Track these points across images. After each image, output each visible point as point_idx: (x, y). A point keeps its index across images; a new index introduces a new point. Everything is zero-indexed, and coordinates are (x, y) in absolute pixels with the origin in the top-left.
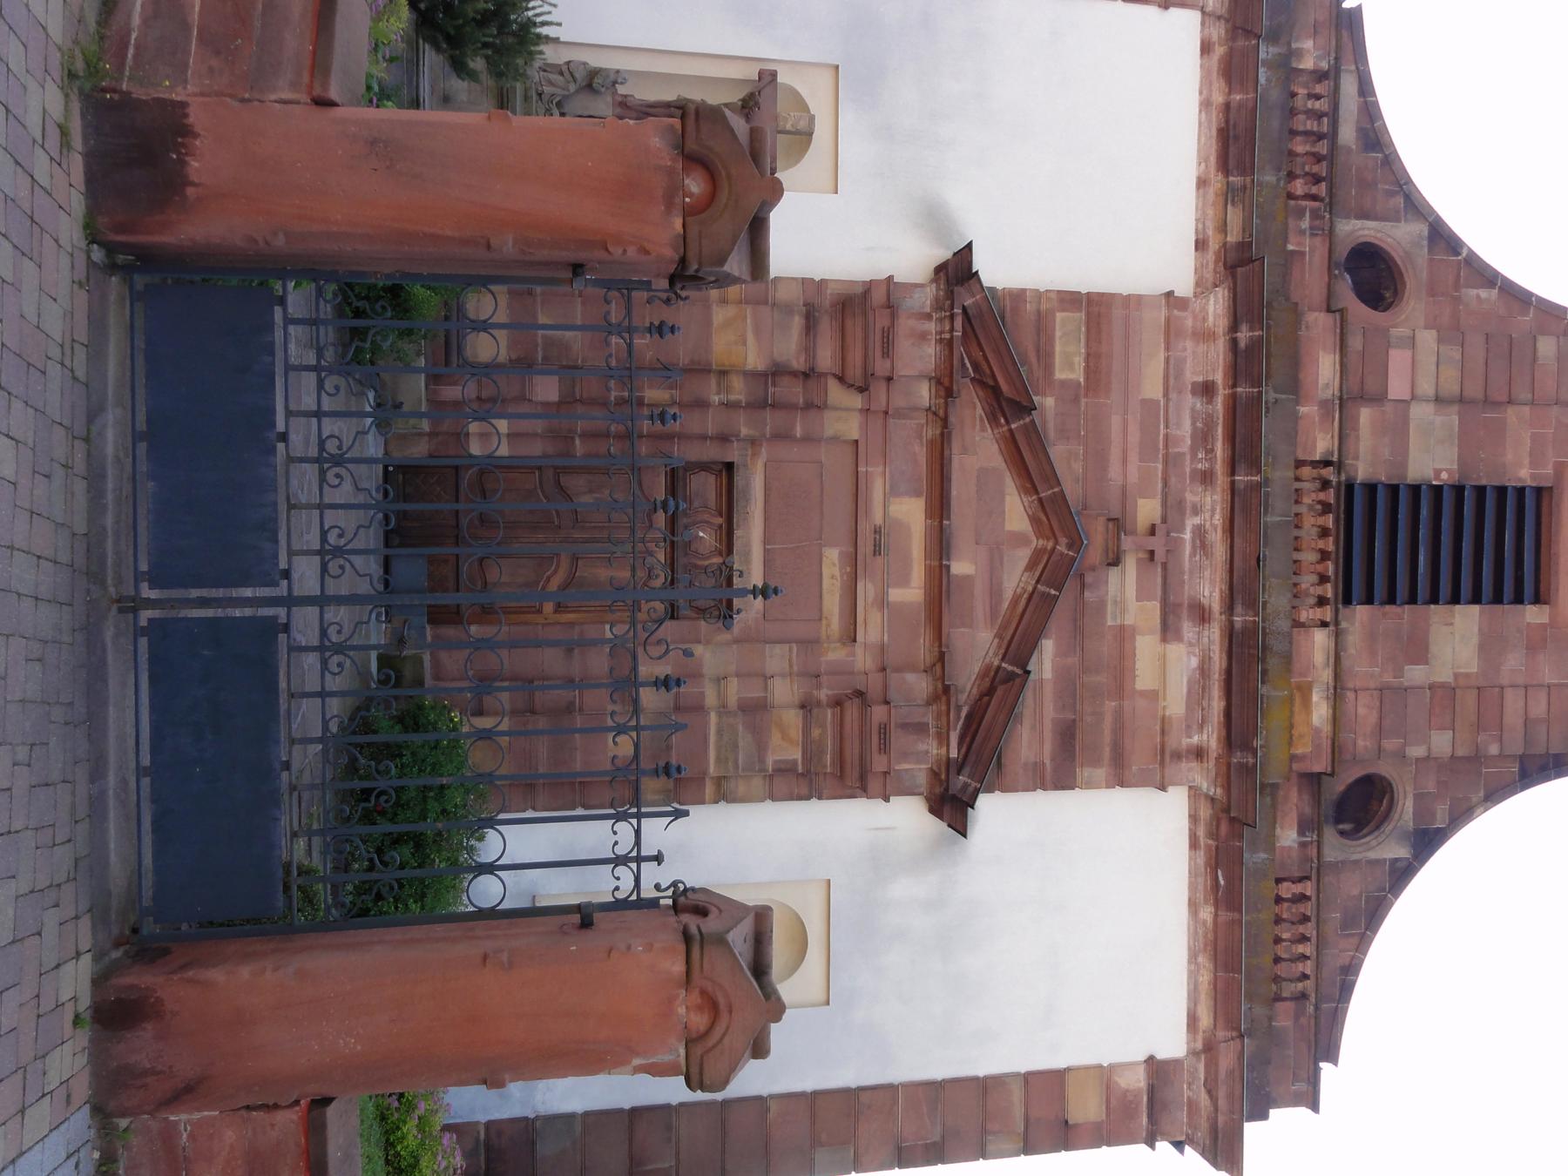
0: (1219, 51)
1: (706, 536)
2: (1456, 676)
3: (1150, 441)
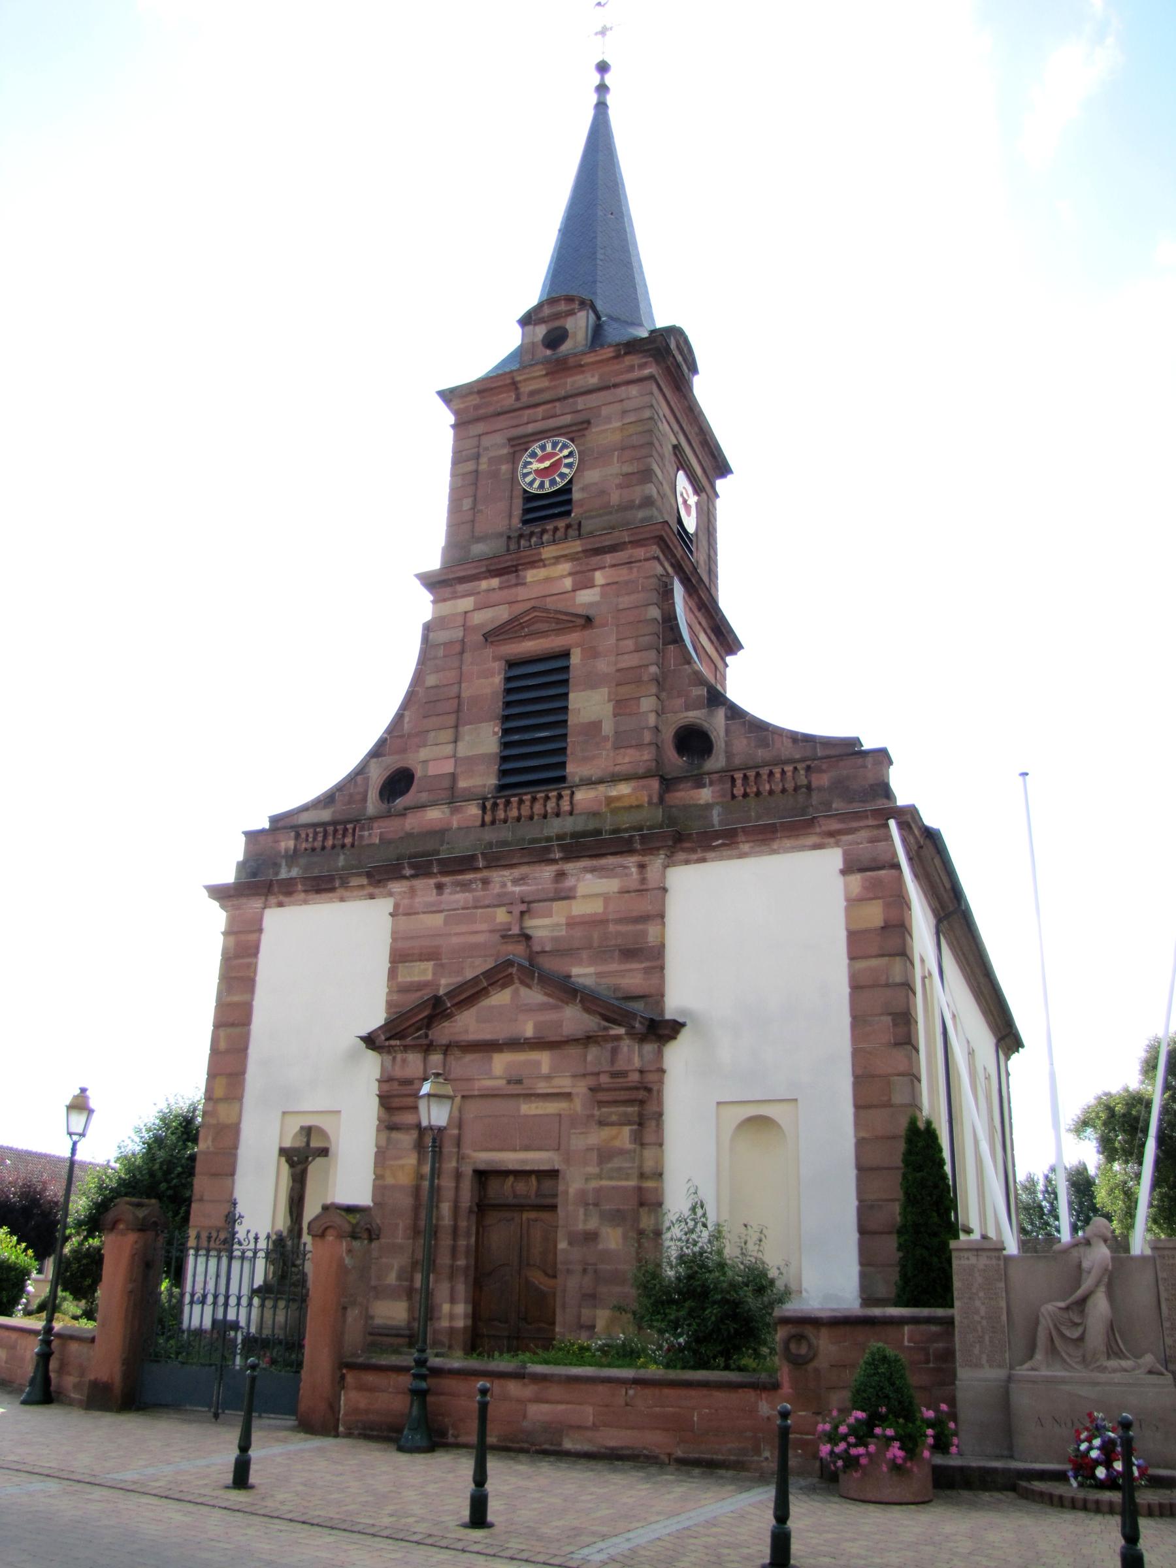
0: (281, 898)
1: (521, 1187)
2: (609, 701)
3: (466, 919)
